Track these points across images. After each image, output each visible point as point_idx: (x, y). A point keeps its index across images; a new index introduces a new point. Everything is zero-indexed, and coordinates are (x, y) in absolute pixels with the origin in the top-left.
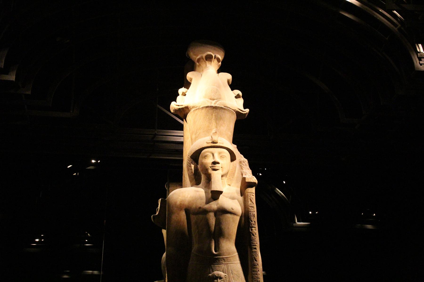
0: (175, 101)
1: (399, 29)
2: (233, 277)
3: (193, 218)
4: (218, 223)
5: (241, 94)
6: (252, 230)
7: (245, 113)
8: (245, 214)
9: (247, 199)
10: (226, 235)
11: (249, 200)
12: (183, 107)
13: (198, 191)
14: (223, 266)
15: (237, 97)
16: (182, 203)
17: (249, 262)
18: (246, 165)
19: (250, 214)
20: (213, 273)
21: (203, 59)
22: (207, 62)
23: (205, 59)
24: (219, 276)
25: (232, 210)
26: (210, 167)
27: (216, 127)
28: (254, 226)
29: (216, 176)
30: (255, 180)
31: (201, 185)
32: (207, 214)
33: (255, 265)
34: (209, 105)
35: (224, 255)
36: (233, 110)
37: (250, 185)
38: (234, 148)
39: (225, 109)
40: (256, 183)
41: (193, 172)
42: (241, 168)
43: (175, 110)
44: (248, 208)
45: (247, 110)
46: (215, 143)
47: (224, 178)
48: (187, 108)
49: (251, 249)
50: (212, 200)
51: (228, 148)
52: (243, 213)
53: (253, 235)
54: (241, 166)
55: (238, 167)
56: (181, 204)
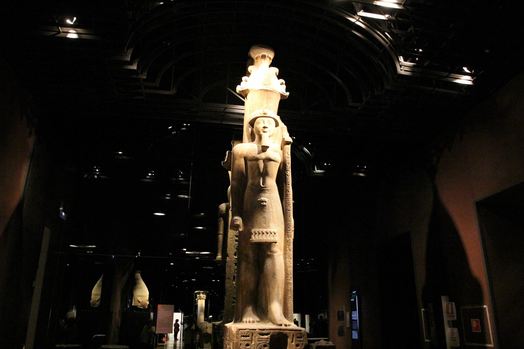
3: (249, 163)
4: (265, 167)
5: (284, 82)
6: (287, 172)
8: (283, 162)
9: (285, 152)
10: (270, 175)
11: (286, 153)
12: (245, 89)
13: (252, 146)
15: (282, 84)
17: (284, 192)
18: (285, 130)
20: (260, 199)
21: (260, 57)
22: (262, 59)
23: (261, 58)
25: (274, 159)
29: (264, 136)
35: (269, 188)
37: (288, 143)
38: (278, 118)
41: (250, 133)
44: (285, 158)
45: (288, 94)
46: (265, 114)
47: (270, 138)
48: (247, 90)
49: (286, 184)
50: (261, 151)
51: (275, 119)
53: (288, 176)
56: (241, 154)
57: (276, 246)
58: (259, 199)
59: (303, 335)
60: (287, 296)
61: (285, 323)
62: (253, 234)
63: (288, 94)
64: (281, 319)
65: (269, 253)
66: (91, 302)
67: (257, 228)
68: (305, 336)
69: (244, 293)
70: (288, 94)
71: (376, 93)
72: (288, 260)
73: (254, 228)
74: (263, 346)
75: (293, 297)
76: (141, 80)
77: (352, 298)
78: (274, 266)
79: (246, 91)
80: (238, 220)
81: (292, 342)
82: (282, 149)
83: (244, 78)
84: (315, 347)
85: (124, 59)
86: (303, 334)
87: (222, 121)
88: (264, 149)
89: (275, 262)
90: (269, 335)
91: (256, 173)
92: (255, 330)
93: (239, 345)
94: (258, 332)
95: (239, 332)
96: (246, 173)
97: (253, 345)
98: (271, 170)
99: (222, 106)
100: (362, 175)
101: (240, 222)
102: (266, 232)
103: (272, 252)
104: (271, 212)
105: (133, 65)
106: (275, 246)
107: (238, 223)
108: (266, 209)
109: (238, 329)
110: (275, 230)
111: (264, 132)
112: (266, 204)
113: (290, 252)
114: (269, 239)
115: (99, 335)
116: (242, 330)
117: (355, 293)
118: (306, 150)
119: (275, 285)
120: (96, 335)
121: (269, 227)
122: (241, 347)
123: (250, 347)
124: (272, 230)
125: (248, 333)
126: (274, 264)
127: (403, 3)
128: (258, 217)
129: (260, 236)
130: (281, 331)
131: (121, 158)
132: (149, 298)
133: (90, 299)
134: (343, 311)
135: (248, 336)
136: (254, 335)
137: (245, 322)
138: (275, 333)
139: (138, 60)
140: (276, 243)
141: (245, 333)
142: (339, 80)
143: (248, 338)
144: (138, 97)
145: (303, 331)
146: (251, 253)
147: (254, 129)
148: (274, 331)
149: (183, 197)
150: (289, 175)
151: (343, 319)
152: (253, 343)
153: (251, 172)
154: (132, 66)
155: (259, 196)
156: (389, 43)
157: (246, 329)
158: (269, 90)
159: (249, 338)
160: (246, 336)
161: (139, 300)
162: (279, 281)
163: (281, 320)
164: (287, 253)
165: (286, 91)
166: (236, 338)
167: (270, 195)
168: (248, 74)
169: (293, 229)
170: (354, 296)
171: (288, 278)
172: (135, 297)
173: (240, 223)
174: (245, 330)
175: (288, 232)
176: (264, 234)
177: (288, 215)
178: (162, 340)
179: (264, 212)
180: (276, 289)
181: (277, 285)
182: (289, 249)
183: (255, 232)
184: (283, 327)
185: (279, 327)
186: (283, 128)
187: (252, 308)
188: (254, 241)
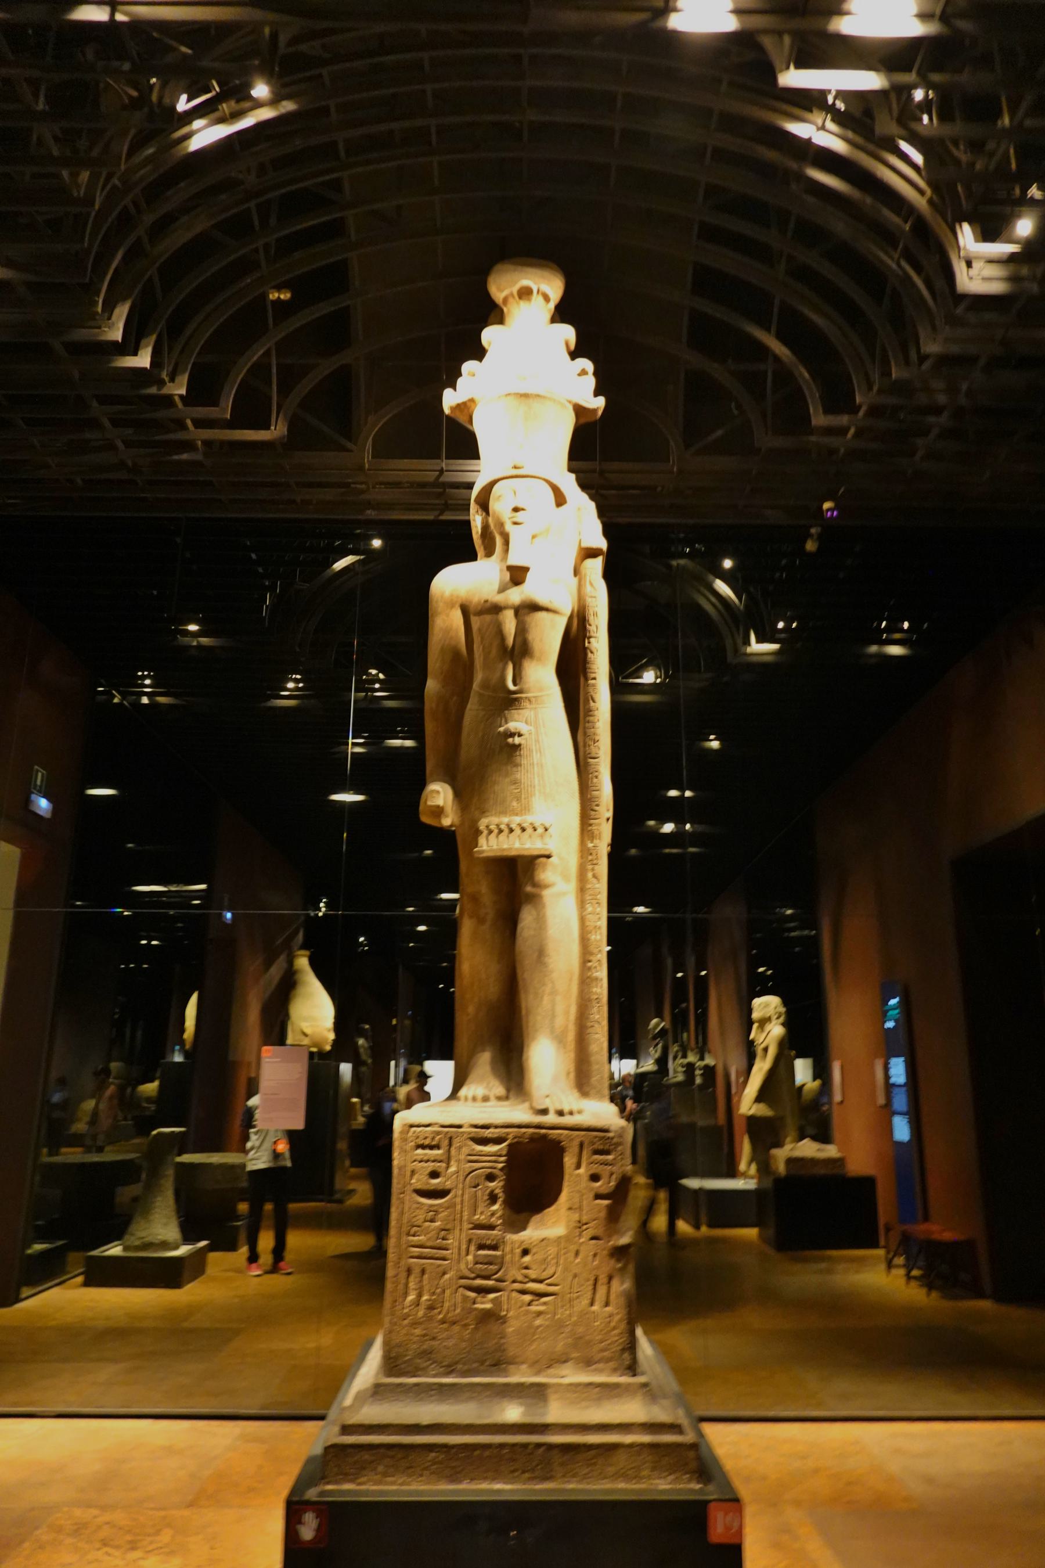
1: (930, 202)
3: (476, 622)
4: (522, 630)
6: (589, 643)
8: (578, 611)
9: (583, 582)
15: (583, 373)
20: (506, 726)
24: (517, 731)
31: (494, 557)
32: (500, 613)
33: (591, 711)
37: (590, 553)
38: (569, 483)
39: (544, 397)
48: (472, 400)
49: (586, 679)
50: (510, 584)
53: (592, 652)
56: (452, 595)
58: (502, 729)
59: (615, 1144)
62: (482, 833)
63: (600, 403)
65: (529, 889)
67: (495, 815)
70: (600, 403)
71: (896, 373)
73: (488, 814)
74: (483, 1177)
76: (177, 398)
79: (468, 404)
80: (438, 792)
82: (576, 572)
83: (468, 367)
85: (103, 338)
86: (615, 1140)
87: (441, 514)
88: (517, 575)
89: (544, 916)
91: (494, 652)
92: (460, 1127)
93: (408, 1173)
95: (408, 1132)
96: (468, 653)
99: (429, 467)
100: (895, 650)
103: (536, 885)
104: (537, 764)
106: (545, 864)
107: (440, 801)
108: (520, 755)
109: (405, 1125)
111: (515, 523)
113: (597, 886)
116: (418, 1126)
121: (529, 810)
122: (413, 1181)
126: (541, 922)
127: (938, 12)
129: (502, 837)
131: (195, 643)
135: (437, 1147)
136: (456, 1143)
139: (154, 337)
140: (549, 857)
141: (426, 1138)
144: (185, 456)
145: (616, 1132)
147: (490, 519)
148: (520, 1132)
149: (399, 745)
152: (453, 1169)
153: (481, 647)
163: (547, 1096)
165: (596, 394)
167: (536, 716)
168: (479, 353)
169: (610, 814)
173: (445, 802)
175: (591, 825)
176: (513, 833)
181: (550, 985)
182: (594, 876)
184: (551, 1119)
188: (485, 855)
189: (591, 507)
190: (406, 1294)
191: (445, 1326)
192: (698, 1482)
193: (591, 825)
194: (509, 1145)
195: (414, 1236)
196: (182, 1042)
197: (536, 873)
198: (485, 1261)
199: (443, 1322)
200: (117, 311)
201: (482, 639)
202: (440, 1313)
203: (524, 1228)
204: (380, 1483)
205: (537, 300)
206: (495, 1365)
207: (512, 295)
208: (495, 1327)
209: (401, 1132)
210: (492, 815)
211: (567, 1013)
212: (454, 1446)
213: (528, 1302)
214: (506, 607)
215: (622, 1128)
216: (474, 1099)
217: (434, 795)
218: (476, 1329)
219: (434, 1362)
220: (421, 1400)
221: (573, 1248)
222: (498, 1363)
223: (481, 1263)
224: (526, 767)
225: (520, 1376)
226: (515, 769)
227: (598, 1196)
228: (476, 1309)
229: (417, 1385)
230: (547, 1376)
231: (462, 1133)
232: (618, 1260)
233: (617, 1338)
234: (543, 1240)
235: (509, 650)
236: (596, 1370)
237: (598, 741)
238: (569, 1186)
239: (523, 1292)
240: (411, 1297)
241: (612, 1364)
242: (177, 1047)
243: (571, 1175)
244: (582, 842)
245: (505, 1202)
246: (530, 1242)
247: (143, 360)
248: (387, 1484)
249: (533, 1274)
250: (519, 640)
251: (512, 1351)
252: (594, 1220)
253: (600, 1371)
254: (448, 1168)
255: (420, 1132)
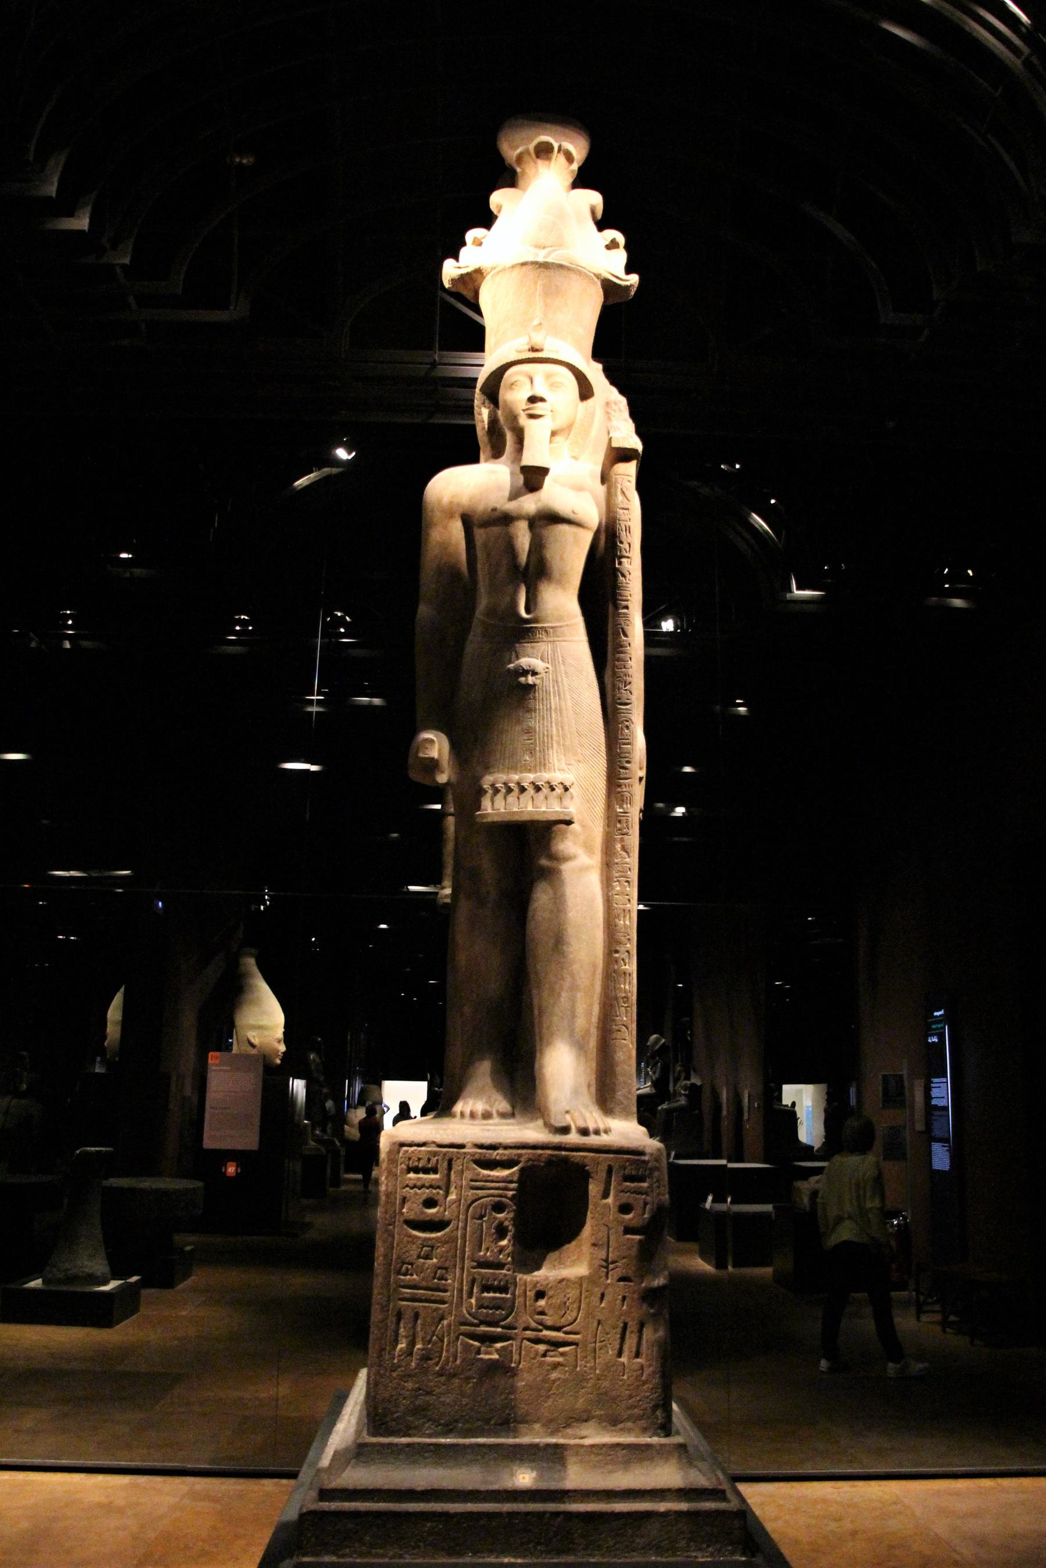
0: (456, 257)
2: (566, 673)
3: (480, 534)
4: (538, 546)
5: (620, 238)
6: (620, 563)
7: (627, 286)
9: (613, 490)
10: (556, 574)
12: (469, 270)
13: (494, 472)
14: (543, 647)
15: (612, 245)
16: (455, 500)
17: (610, 638)
18: (620, 410)
19: (620, 525)
20: (517, 662)
21: (530, 154)
22: (539, 162)
23: (533, 155)
25: (572, 516)
26: (522, 412)
27: (545, 314)
28: (627, 554)
29: (536, 433)
30: (636, 443)
31: (504, 458)
33: (622, 646)
34: (531, 259)
35: (548, 622)
36: (595, 275)
37: (622, 455)
38: (595, 372)
39: (568, 269)
40: (637, 451)
41: (486, 426)
42: (608, 417)
43: (452, 280)
44: (616, 512)
45: (634, 279)
46: (537, 350)
47: (557, 438)
48: (479, 272)
49: (616, 607)
50: (524, 490)
51: (572, 365)
52: (604, 522)
53: (623, 576)
54: (608, 413)
55: (599, 414)
56: (451, 502)
57: (570, 837)
58: (511, 666)
60: (614, 1020)
61: (581, 1124)
62: (486, 792)
63: (634, 279)
64: (567, 1108)
65: (544, 862)
66: (106, 1044)
68: (656, 1174)
69: (467, 1010)
72: (618, 888)
74: (490, 1207)
75: (634, 1026)
76: (118, 270)
77: (932, 1035)
78: (559, 911)
79: (474, 275)
80: (432, 741)
81: (606, 1195)
82: (604, 478)
84: (808, 1193)
89: (563, 895)
90: (515, 1168)
91: (503, 572)
92: (462, 1146)
94: (473, 1155)
95: (399, 1152)
97: (454, 1202)
98: (558, 558)
101: (440, 750)
102: (533, 783)
104: (556, 708)
105: (76, 213)
107: (435, 754)
108: (534, 698)
109: (394, 1144)
110: (568, 777)
111: (532, 416)
112: (538, 682)
113: (628, 860)
114: (543, 809)
115: (93, 1149)
116: (410, 1145)
117: (940, 1016)
118: (757, 520)
119: (563, 979)
120: (83, 1148)
121: (545, 765)
122: (404, 1210)
123: (442, 1209)
124: (556, 776)
125: (434, 1160)
126: (559, 903)
128: (507, 731)
129: (511, 798)
130: (563, 1153)
132: (284, 1033)
133: (105, 1037)
134: (901, 1076)
135: (435, 1171)
136: (457, 1166)
137: (458, 1115)
138: (538, 1160)
140: (569, 823)
142: (840, 231)
143: (432, 1176)
145: (651, 1155)
146: (487, 865)
147: (500, 412)
150: (627, 574)
151: (902, 1104)
152: (452, 1197)
154: (72, 219)
155: (514, 654)
156: (1026, 50)
157: (424, 1144)
158: (553, 263)
159: (437, 1176)
160: (426, 1171)
161: (253, 1041)
162: (576, 967)
163: (567, 1112)
164: (616, 861)
166: (387, 1178)
167: (554, 651)
168: (487, 219)
169: (643, 773)
170: (939, 1026)
171: (617, 955)
172: (238, 1028)
174: (423, 1148)
175: (620, 786)
177: (622, 722)
178: (239, 1171)
179: (529, 711)
180: (564, 994)
181: (569, 980)
182: (624, 848)
183: (493, 785)
184: (574, 1138)
185: (558, 1139)
186: (614, 407)
187: (492, 1067)
188: (489, 820)
189: (621, 402)
190: (396, 1342)
191: (443, 1379)
192: (743, 1554)
193: (620, 786)
194: (522, 1170)
195: (405, 1274)
196: (102, 1051)
197: (554, 842)
198: (491, 1305)
199: (440, 1374)
200: (52, 163)
201: (489, 555)
202: (437, 1364)
203: (538, 1268)
204: (368, 1554)
205: (559, 160)
206: (501, 1424)
207: (527, 152)
208: (501, 1381)
209: (390, 1153)
210: (498, 771)
211: (589, 1013)
212: (456, 1514)
213: (542, 1352)
214: (518, 518)
215: (659, 1150)
216: (473, 1115)
217: (427, 745)
218: (480, 1382)
219: (429, 1420)
220: (414, 1462)
221: (598, 1291)
222: (508, 1422)
223: (486, 1308)
224: (541, 714)
225: (533, 1436)
226: (528, 715)
227: (628, 1230)
228: (481, 1359)
229: (409, 1445)
230: (563, 1437)
231: (465, 1153)
232: (651, 1306)
233: (648, 1392)
234: (562, 1280)
235: (521, 570)
236: (621, 1430)
237: (630, 683)
238: (592, 1218)
239: (537, 1341)
240: (402, 1345)
241: (643, 1423)
242: (98, 1059)
243: (596, 1205)
244: (609, 807)
245: (514, 1237)
246: (545, 1283)
247: (82, 223)
248: (377, 1556)
249: (548, 1320)
250: (533, 558)
251: (523, 1409)
252: (624, 1258)
253: (629, 1431)
254: (447, 1193)
255: (413, 1152)
